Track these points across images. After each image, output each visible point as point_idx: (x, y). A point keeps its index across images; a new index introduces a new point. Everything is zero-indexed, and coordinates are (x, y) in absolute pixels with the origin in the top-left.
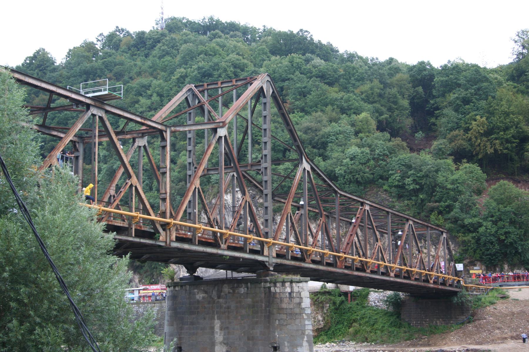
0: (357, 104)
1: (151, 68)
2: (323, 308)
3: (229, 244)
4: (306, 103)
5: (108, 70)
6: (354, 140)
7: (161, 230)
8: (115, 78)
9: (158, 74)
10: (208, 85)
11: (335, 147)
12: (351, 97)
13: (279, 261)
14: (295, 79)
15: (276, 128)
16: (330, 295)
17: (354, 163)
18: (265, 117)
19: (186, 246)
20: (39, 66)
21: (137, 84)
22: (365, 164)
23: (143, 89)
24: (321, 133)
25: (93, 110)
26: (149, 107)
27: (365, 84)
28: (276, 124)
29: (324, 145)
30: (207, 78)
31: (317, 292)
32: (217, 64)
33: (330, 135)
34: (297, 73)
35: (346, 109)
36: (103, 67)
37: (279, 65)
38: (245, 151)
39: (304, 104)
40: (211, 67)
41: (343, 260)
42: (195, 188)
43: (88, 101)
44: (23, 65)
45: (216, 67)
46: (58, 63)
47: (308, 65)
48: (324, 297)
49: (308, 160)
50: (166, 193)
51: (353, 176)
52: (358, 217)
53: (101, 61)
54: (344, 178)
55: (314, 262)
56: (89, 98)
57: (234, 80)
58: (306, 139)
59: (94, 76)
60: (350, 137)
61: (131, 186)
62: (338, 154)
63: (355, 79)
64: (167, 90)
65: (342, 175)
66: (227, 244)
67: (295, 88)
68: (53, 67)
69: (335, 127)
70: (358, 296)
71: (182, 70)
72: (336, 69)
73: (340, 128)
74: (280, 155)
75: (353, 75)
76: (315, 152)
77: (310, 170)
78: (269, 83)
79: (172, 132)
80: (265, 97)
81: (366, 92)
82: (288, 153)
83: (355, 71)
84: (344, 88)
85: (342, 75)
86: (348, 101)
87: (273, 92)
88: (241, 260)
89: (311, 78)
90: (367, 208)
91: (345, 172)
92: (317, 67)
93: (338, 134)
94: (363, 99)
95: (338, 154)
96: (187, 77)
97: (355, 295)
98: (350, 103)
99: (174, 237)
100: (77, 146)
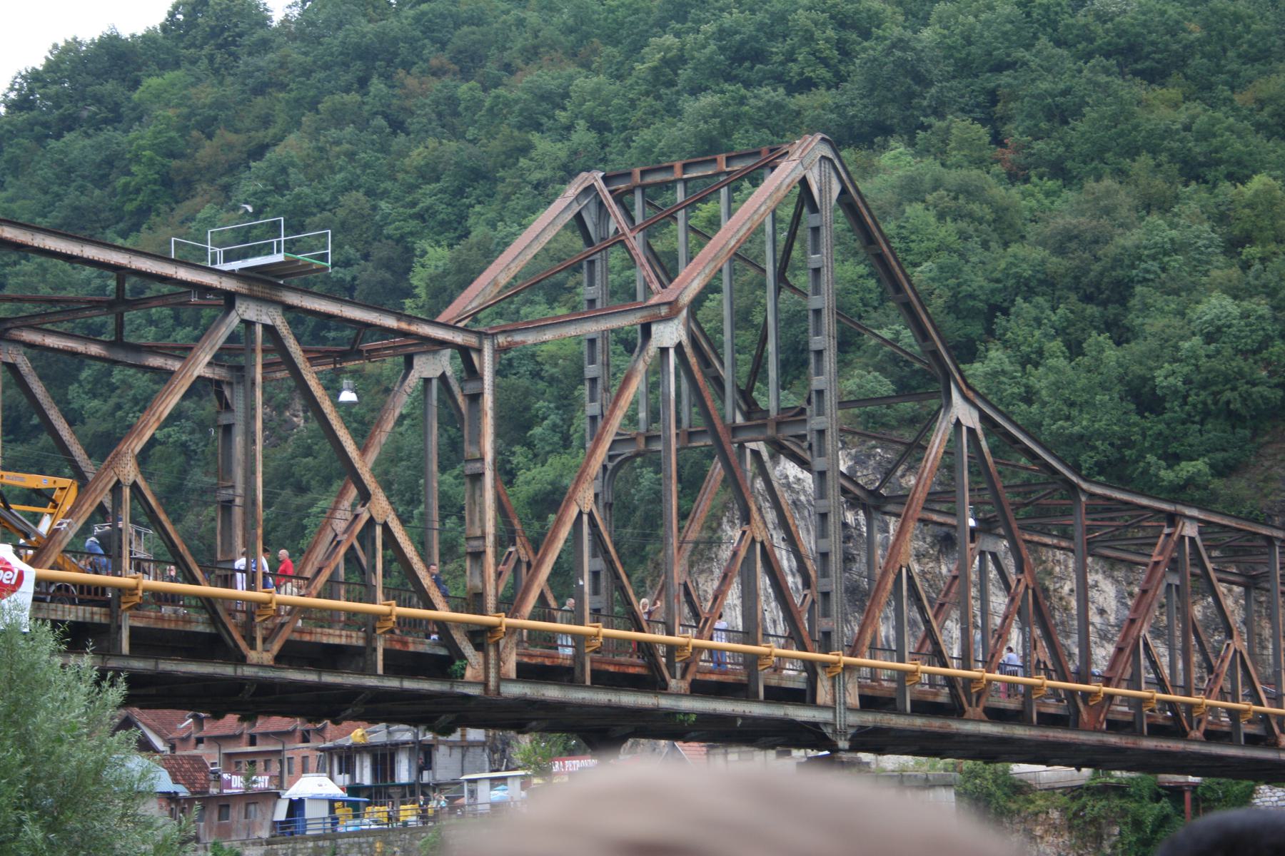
0: (1239, 146)
1: (571, 31)
2: (1099, 838)
3: (699, 677)
4: (1069, 146)
5: (434, 41)
6: (1222, 271)
7: (468, 650)
8: (457, 68)
9: (595, 52)
10: (643, 173)
11: (1158, 299)
12: (1219, 121)
13: (870, 719)
14: (1034, 63)
15: (964, 236)
16: (1121, 797)
17: (1218, 352)
18: (817, 271)
19: (552, 693)
20: (215, 33)
21: (528, 90)
22: (1254, 352)
23: (545, 105)
24: (1111, 250)
25: (246, 310)
26: (564, 167)
27: (1272, 71)
28: (962, 225)
29: (1121, 291)
30: (747, 64)
31: (1080, 787)
32: (781, 18)
33: (1140, 258)
34: (1043, 41)
35: (1201, 165)
36: (418, 33)
37: (983, 17)
38: (860, 317)
39: (1061, 150)
40: (761, 26)
41: (1101, 705)
42: (580, 513)
43: (229, 285)
44: (164, 28)
45: (779, 28)
46: (277, 17)
47: (1082, 12)
48: (1104, 803)
49: (971, 394)
50: (483, 537)
51: (1215, 394)
52: (1157, 563)
53: (412, 13)
54: (1186, 403)
55: (996, 715)
56: (230, 274)
57: (722, 158)
58: (1062, 271)
59: (389, 62)
60: (1208, 263)
61: (371, 522)
62: (1166, 321)
63: (1239, 56)
64: (620, 110)
65: (1176, 392)
66: (689, 678)
67: (1032, 96)
68: (260, 33)
69: (1159, 228)
70: (1219, 800)
71: (669, 39)
72: (1177, 22)
73: (1174, 233)
74: (976, 329)
75: (1234, 40)
76: (1092, 315)
77: (978, 427)
78: (827, 165)
79: (499, 351)
80: (814, 209)
81: (1272, 100)
82: (1000, 320)
83: (1240, 27)
84: (1202, 89)
85: (1199, 41)
86: (1204, 136)
87: (844, 191)
88: (739, 722)
89: (1088, 56)
90: (1190, 530)
91: (1187, 381)
92: (1111, 20)
93: (1166, 254)
94: (1259, 127)
95: (1166, 321)
96: (685, 62)
97: (1208, 795)
98: (1216, 142)
99: (510, 668)
100: (227, 393)
